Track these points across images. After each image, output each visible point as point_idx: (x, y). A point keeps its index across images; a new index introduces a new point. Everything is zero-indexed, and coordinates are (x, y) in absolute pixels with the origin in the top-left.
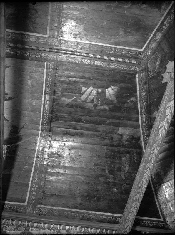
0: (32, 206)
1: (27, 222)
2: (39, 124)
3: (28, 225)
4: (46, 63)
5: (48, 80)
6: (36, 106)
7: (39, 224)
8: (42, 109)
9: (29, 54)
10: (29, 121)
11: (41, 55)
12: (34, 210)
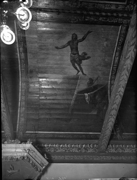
0: (120, 134)
1: (55, 145)
2: (109, 76)
3: (56, 146)
4: (120, 27)
5: (120, 40)
6: (108, 62)
7: (75, 146)
8: (112, 63)
9: (108, 20)
10: (101, 74)
11: (118, 20)
12: (122, 137)
